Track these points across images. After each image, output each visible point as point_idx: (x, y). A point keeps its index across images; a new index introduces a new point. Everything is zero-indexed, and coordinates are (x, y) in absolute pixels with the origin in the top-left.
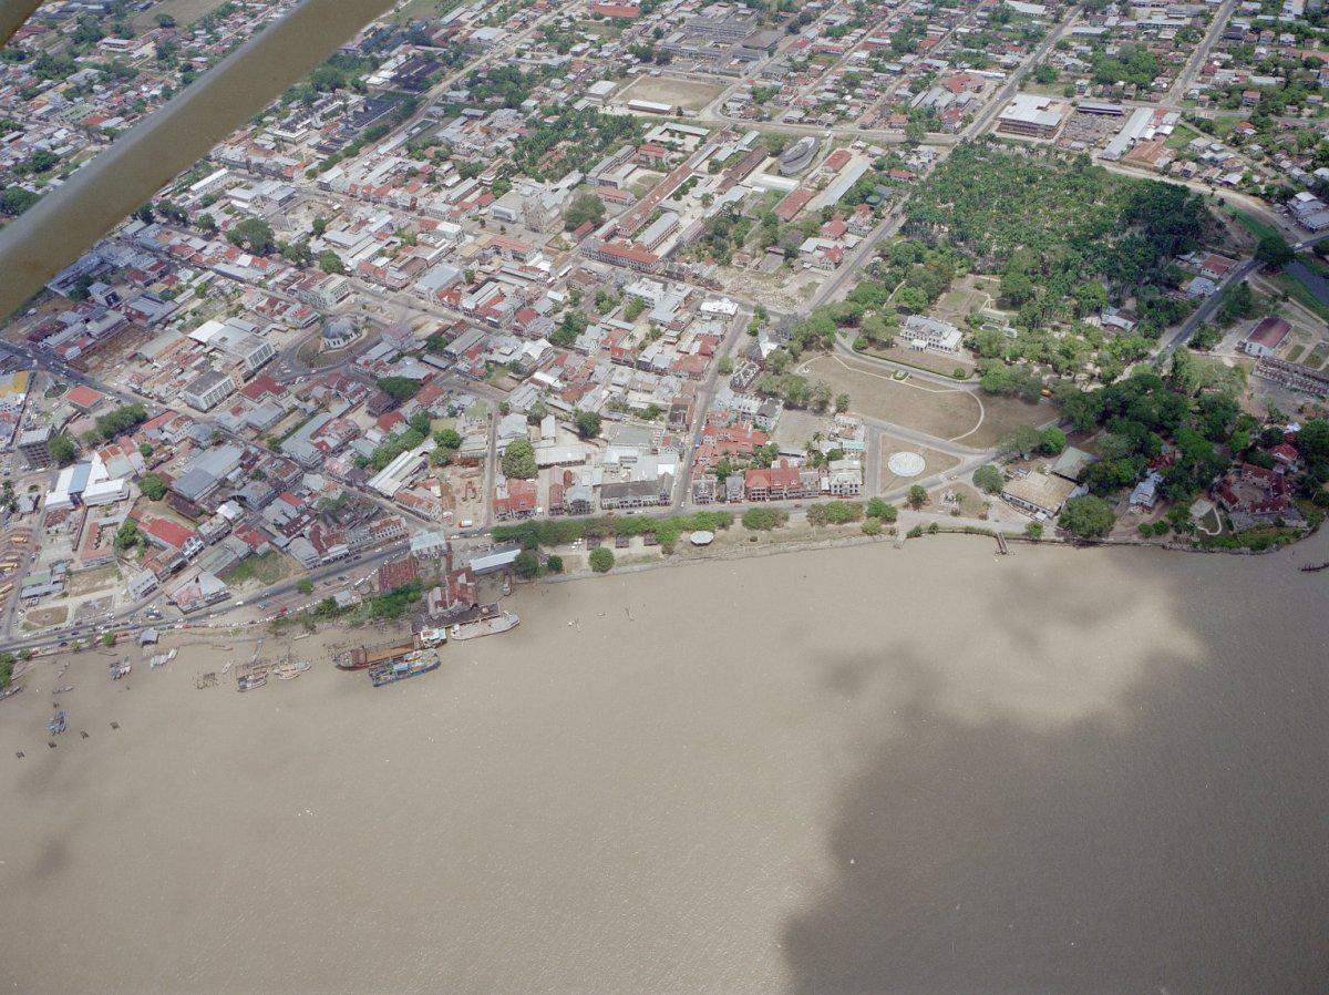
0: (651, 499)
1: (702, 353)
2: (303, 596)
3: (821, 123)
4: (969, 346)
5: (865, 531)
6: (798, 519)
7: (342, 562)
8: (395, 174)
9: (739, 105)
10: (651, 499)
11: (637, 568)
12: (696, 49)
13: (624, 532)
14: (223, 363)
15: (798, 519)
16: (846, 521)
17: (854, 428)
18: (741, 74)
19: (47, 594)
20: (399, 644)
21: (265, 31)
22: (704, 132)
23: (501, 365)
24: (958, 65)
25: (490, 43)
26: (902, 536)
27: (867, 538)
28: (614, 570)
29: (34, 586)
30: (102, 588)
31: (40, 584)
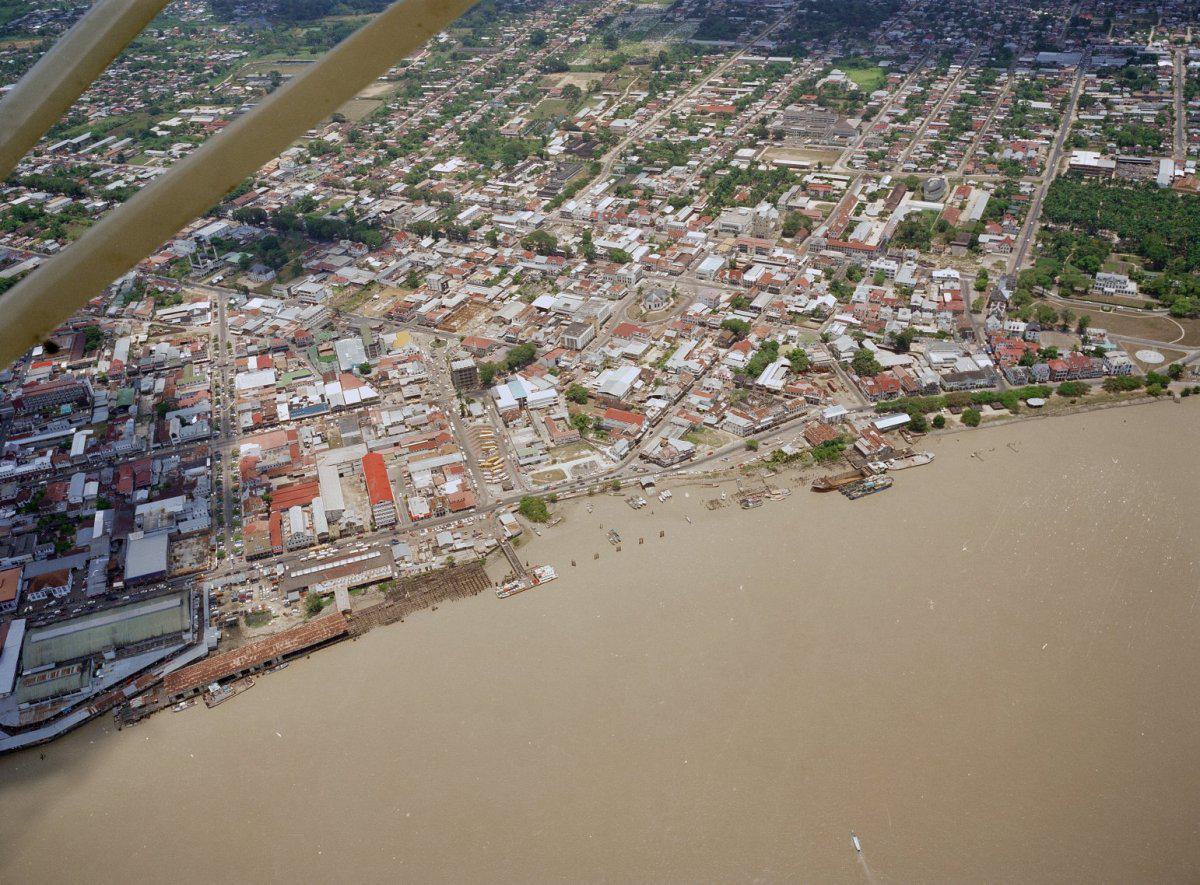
0: (982, 382)
1: (954, 299)
2: (751, 452)
3: (932, 171)
4: (1142, 290)
5: (1150, 393)
6: (1096, 390)
7: (767, 432)
8: (616, 208)
9: (863, 162)
10: (982, 382)
11: (997, 423)
12: (803, 129)
13: (980, 401)
14: (995, 261)
15: (1096, 390)
16: (1133, 388)
17: (1102, 336)
18: (847, 144)
19: (539, 462)
20: (849, 475)
21: (134, 200)
22: (848, 178)
23: (799, 314)
24: (1011, 137)
25: (625, 131)
26: (1178, 396)
27: (1153, 398)
28: (981, 424)
29: (527, 456)
30: (578, 457)
31: (532, 455)
